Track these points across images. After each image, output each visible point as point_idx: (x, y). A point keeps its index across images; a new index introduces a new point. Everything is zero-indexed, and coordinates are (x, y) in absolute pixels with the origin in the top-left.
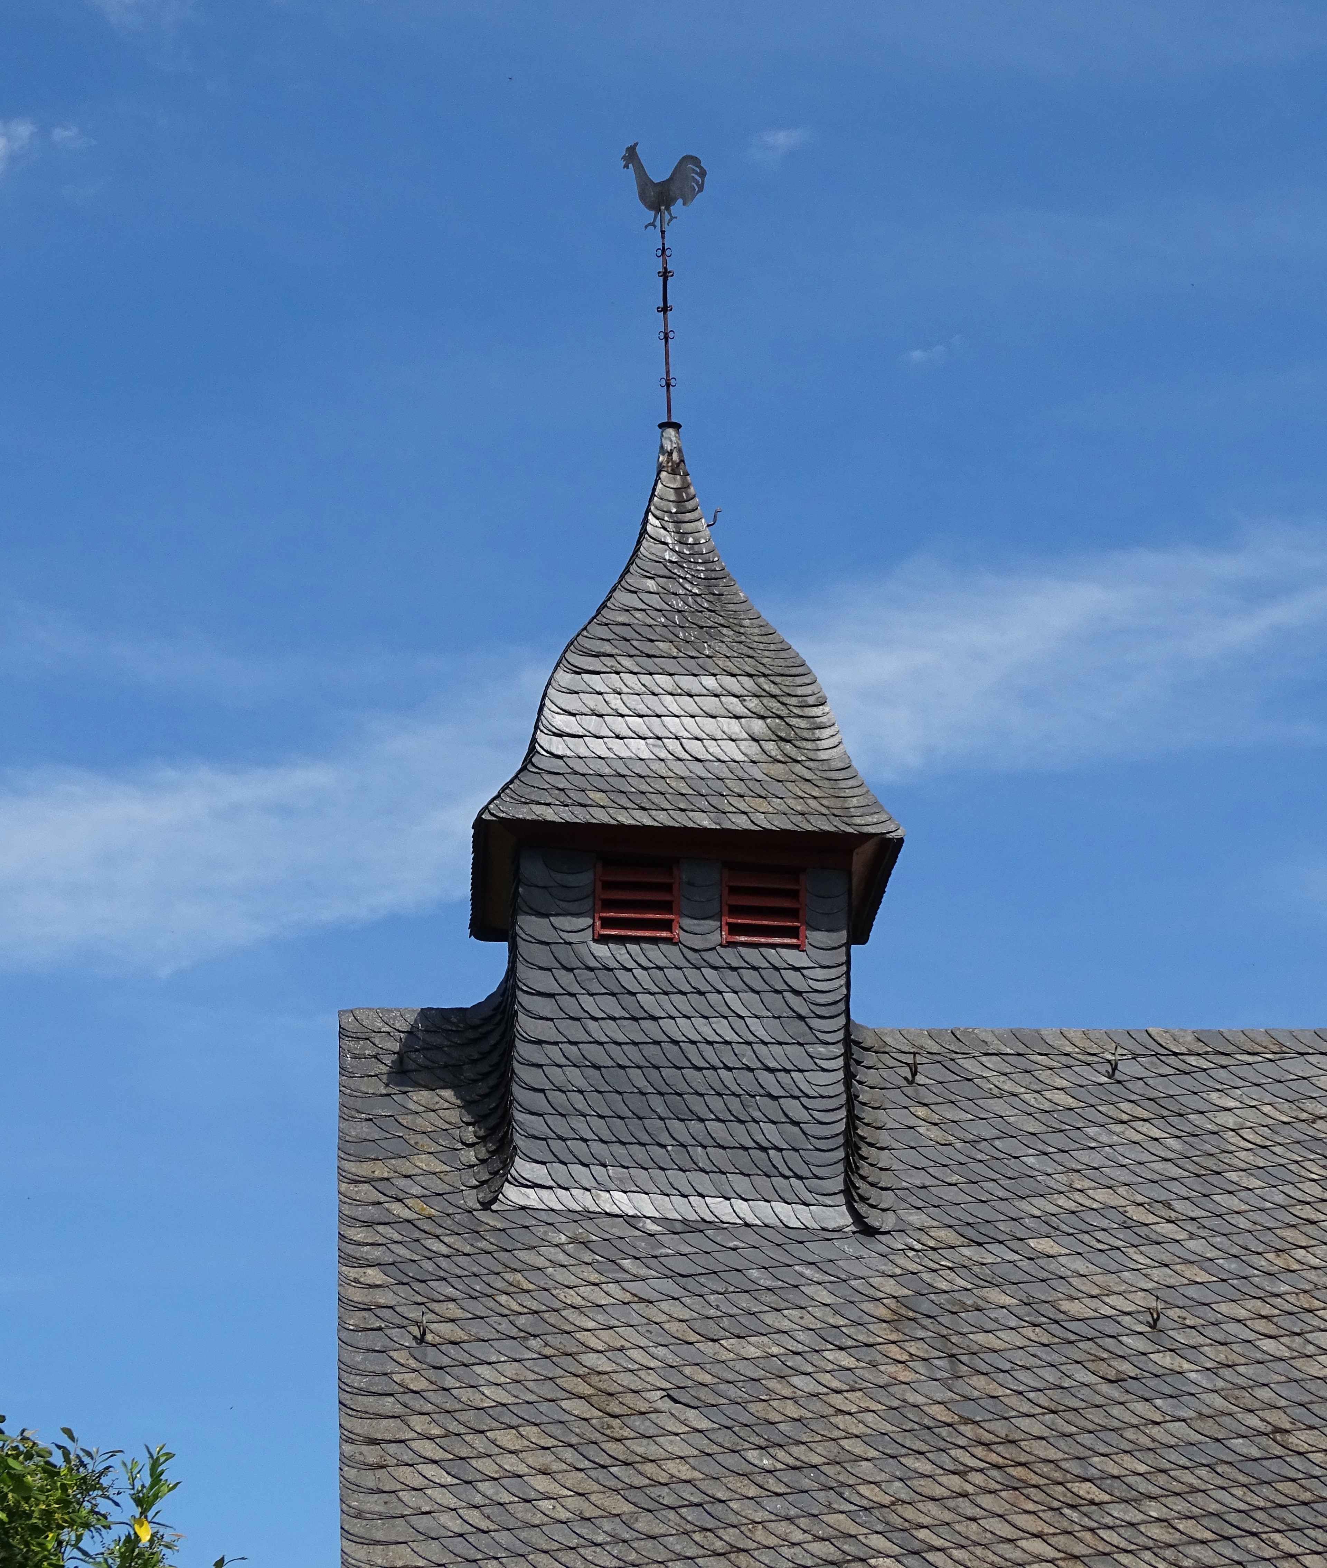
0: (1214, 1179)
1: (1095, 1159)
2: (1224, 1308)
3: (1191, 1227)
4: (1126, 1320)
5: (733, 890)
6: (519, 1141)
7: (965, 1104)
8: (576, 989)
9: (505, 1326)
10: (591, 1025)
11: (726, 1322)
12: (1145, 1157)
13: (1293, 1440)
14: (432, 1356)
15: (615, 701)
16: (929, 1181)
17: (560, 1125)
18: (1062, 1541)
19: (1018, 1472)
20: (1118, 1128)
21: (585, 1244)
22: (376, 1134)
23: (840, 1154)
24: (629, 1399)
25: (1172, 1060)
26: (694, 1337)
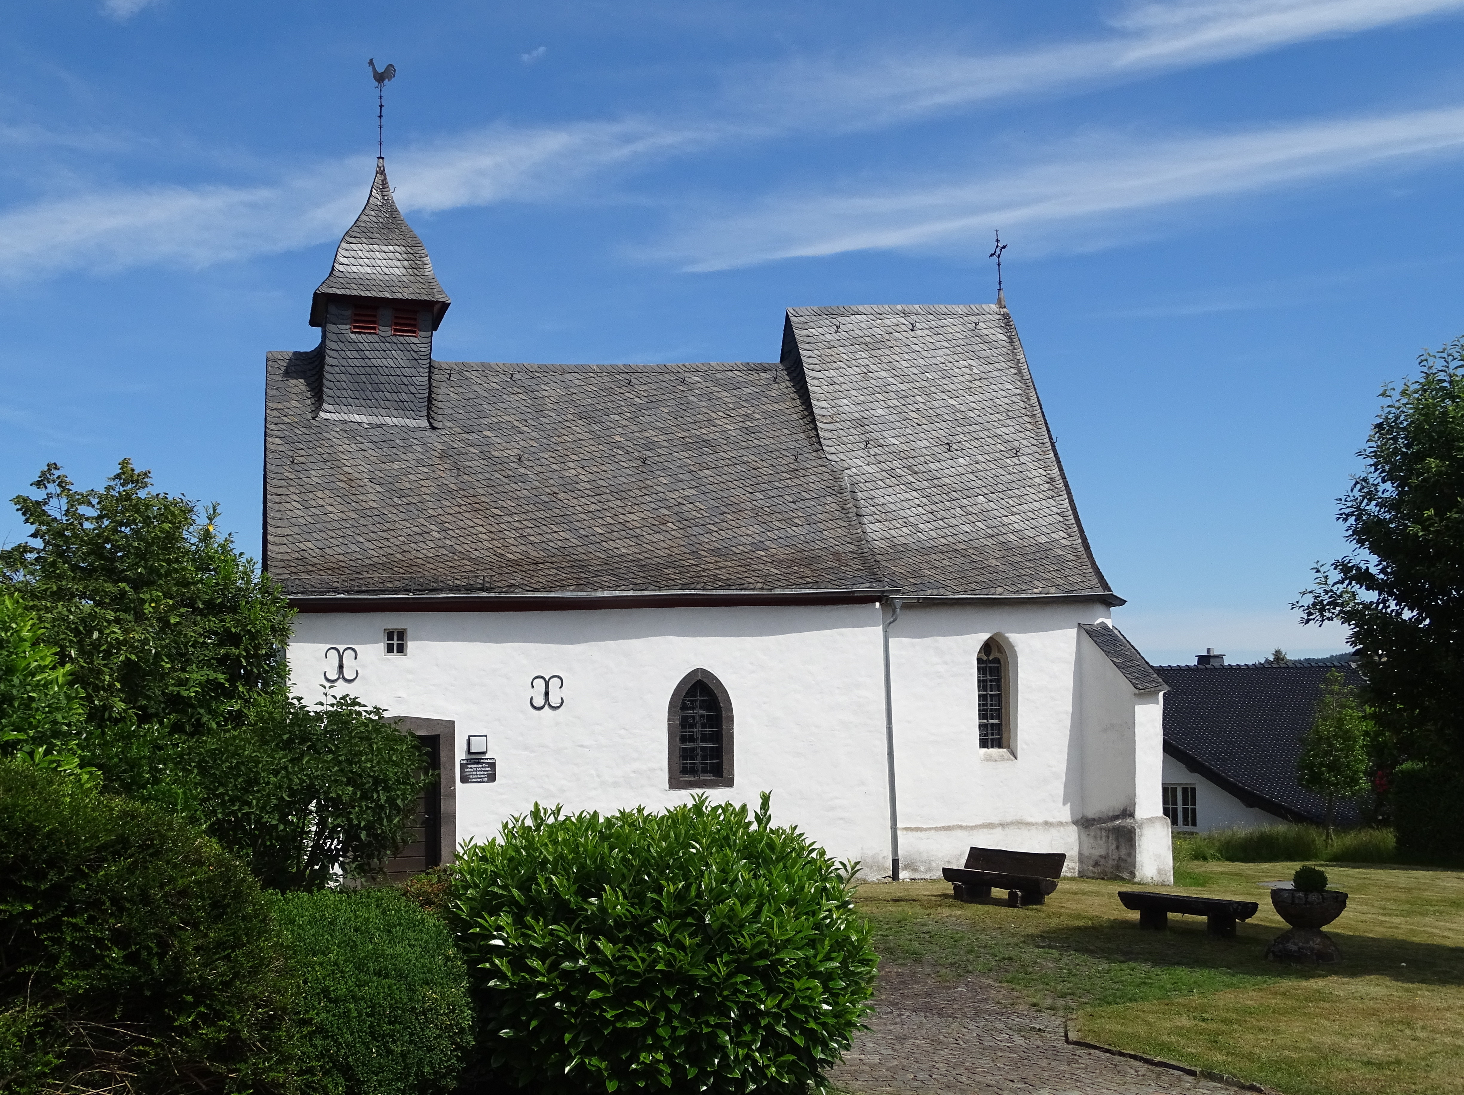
0: (541, 413)
1: (505, 406)
2: (541, 454)
3: (533, 428)
4: (511, 458)
5: (396, 318)
6: (325, 397)
7: (465, 387)
8: (344, 348)
9: (319, 458)
10: (349, 360)
11: (388, 457)
12: (520, 405)
13: (559, 496)
14: (297, 467)
15: (360, 253)
16: (453, 412)
17: (338, 393)
18: (488, 527)
19: (476, 506)
20: (512, 396)
21: (345, 431)
22: (279, 394)
23: (426, 403)
24: (358, 482)
25: (530, 374)
26: (378, 462)
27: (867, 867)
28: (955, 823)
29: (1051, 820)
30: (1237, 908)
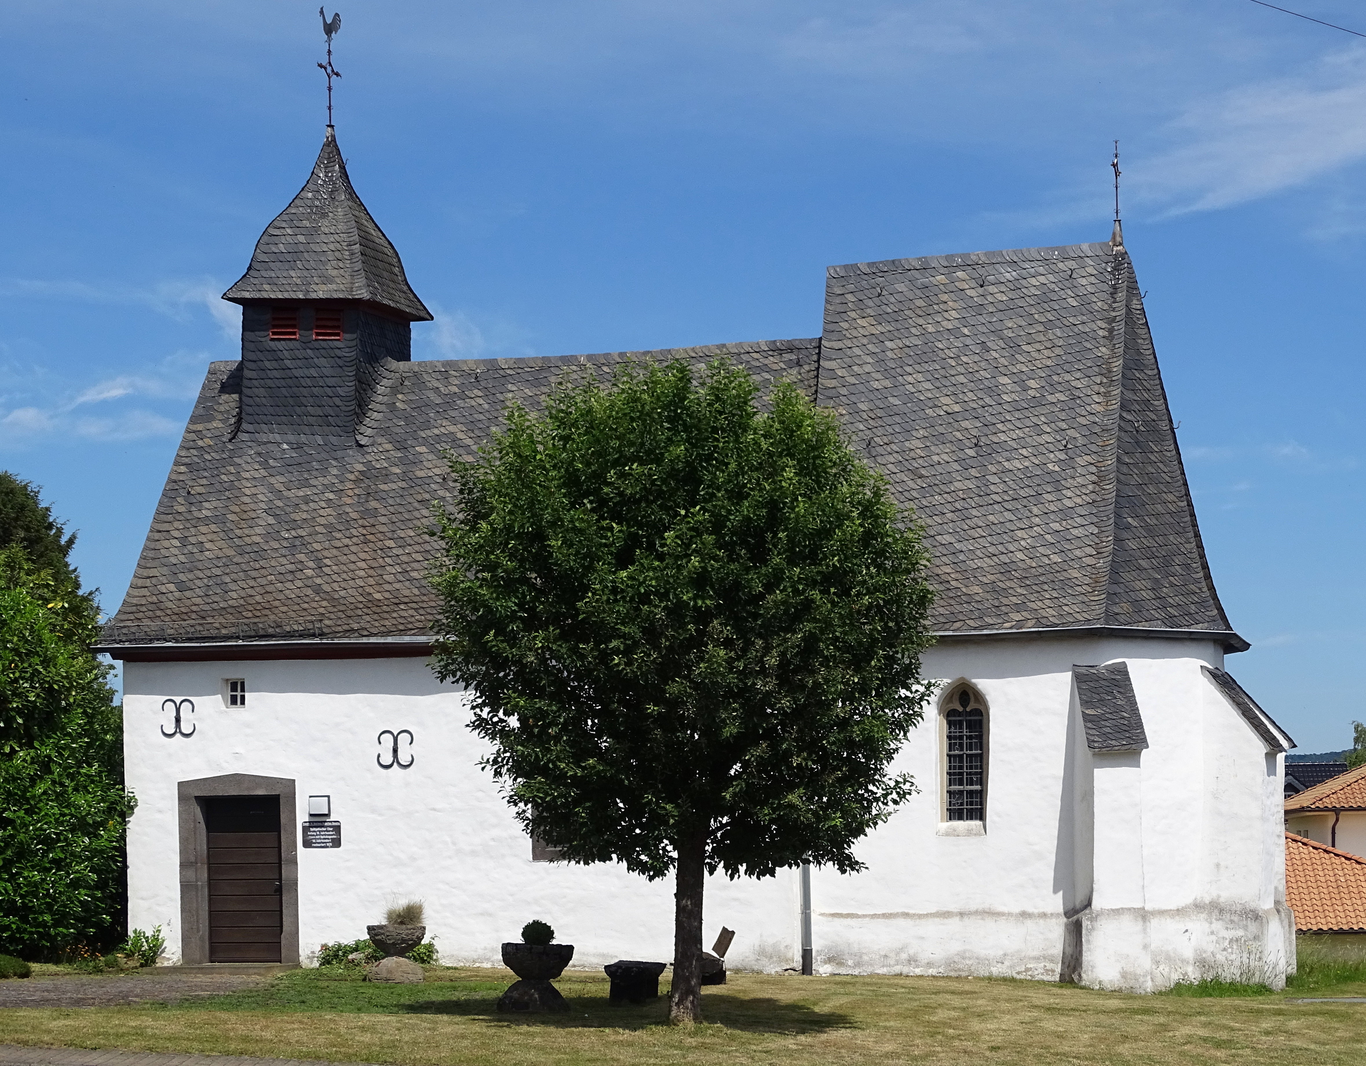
5: (318, 319)
27: (766, 957)
28: (900, 910)
29: (1030, 910)
30: (617, 971)
